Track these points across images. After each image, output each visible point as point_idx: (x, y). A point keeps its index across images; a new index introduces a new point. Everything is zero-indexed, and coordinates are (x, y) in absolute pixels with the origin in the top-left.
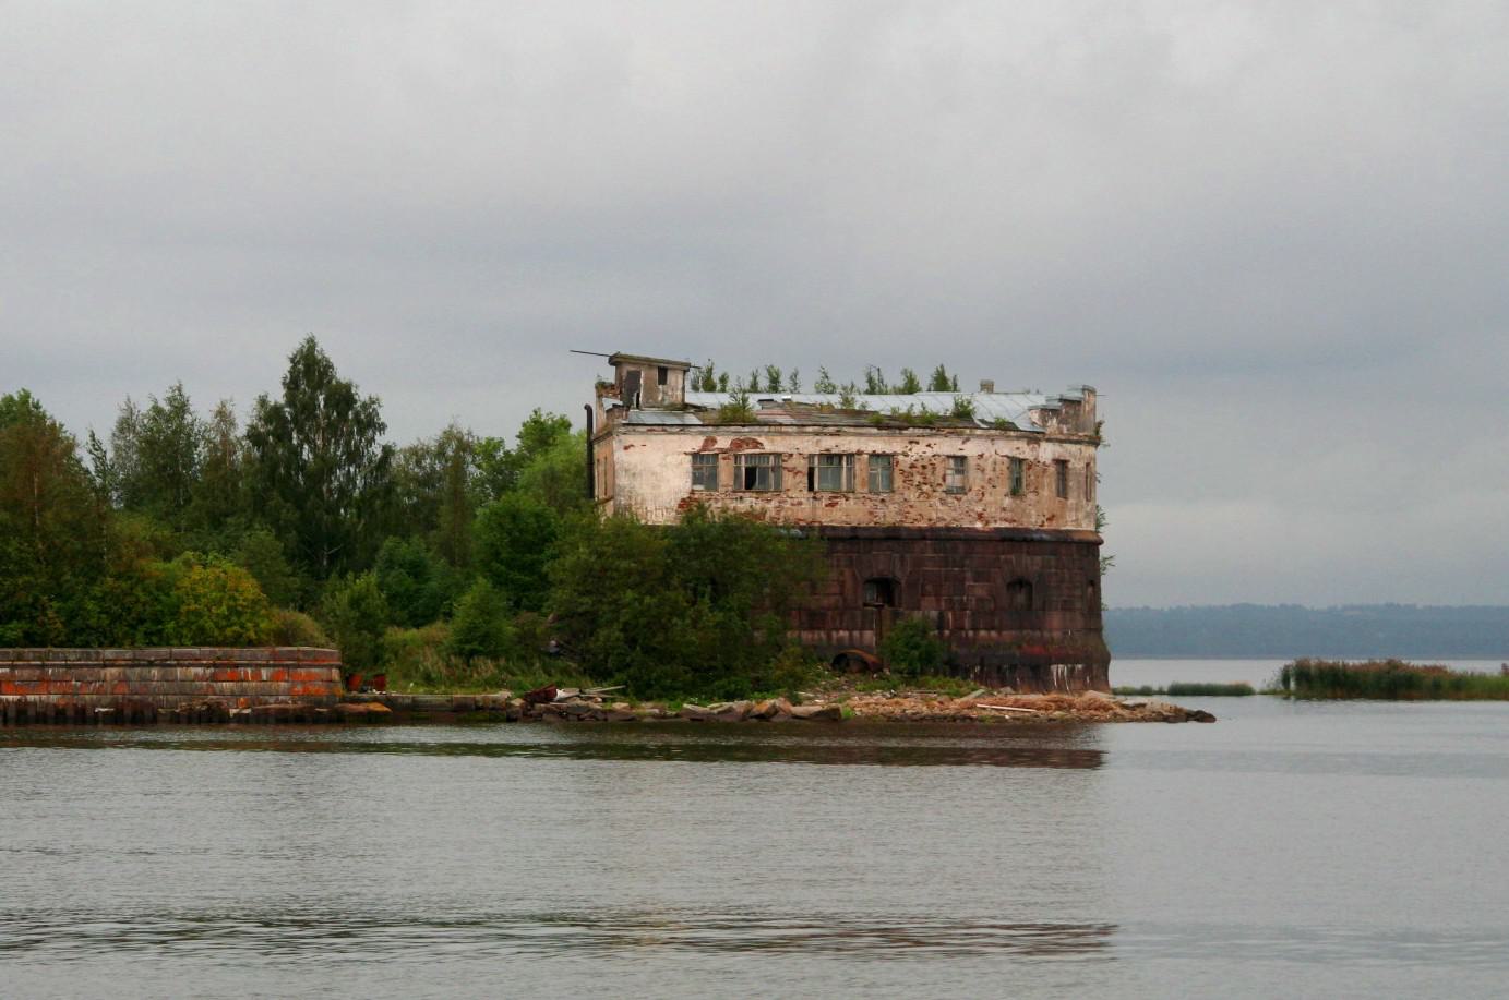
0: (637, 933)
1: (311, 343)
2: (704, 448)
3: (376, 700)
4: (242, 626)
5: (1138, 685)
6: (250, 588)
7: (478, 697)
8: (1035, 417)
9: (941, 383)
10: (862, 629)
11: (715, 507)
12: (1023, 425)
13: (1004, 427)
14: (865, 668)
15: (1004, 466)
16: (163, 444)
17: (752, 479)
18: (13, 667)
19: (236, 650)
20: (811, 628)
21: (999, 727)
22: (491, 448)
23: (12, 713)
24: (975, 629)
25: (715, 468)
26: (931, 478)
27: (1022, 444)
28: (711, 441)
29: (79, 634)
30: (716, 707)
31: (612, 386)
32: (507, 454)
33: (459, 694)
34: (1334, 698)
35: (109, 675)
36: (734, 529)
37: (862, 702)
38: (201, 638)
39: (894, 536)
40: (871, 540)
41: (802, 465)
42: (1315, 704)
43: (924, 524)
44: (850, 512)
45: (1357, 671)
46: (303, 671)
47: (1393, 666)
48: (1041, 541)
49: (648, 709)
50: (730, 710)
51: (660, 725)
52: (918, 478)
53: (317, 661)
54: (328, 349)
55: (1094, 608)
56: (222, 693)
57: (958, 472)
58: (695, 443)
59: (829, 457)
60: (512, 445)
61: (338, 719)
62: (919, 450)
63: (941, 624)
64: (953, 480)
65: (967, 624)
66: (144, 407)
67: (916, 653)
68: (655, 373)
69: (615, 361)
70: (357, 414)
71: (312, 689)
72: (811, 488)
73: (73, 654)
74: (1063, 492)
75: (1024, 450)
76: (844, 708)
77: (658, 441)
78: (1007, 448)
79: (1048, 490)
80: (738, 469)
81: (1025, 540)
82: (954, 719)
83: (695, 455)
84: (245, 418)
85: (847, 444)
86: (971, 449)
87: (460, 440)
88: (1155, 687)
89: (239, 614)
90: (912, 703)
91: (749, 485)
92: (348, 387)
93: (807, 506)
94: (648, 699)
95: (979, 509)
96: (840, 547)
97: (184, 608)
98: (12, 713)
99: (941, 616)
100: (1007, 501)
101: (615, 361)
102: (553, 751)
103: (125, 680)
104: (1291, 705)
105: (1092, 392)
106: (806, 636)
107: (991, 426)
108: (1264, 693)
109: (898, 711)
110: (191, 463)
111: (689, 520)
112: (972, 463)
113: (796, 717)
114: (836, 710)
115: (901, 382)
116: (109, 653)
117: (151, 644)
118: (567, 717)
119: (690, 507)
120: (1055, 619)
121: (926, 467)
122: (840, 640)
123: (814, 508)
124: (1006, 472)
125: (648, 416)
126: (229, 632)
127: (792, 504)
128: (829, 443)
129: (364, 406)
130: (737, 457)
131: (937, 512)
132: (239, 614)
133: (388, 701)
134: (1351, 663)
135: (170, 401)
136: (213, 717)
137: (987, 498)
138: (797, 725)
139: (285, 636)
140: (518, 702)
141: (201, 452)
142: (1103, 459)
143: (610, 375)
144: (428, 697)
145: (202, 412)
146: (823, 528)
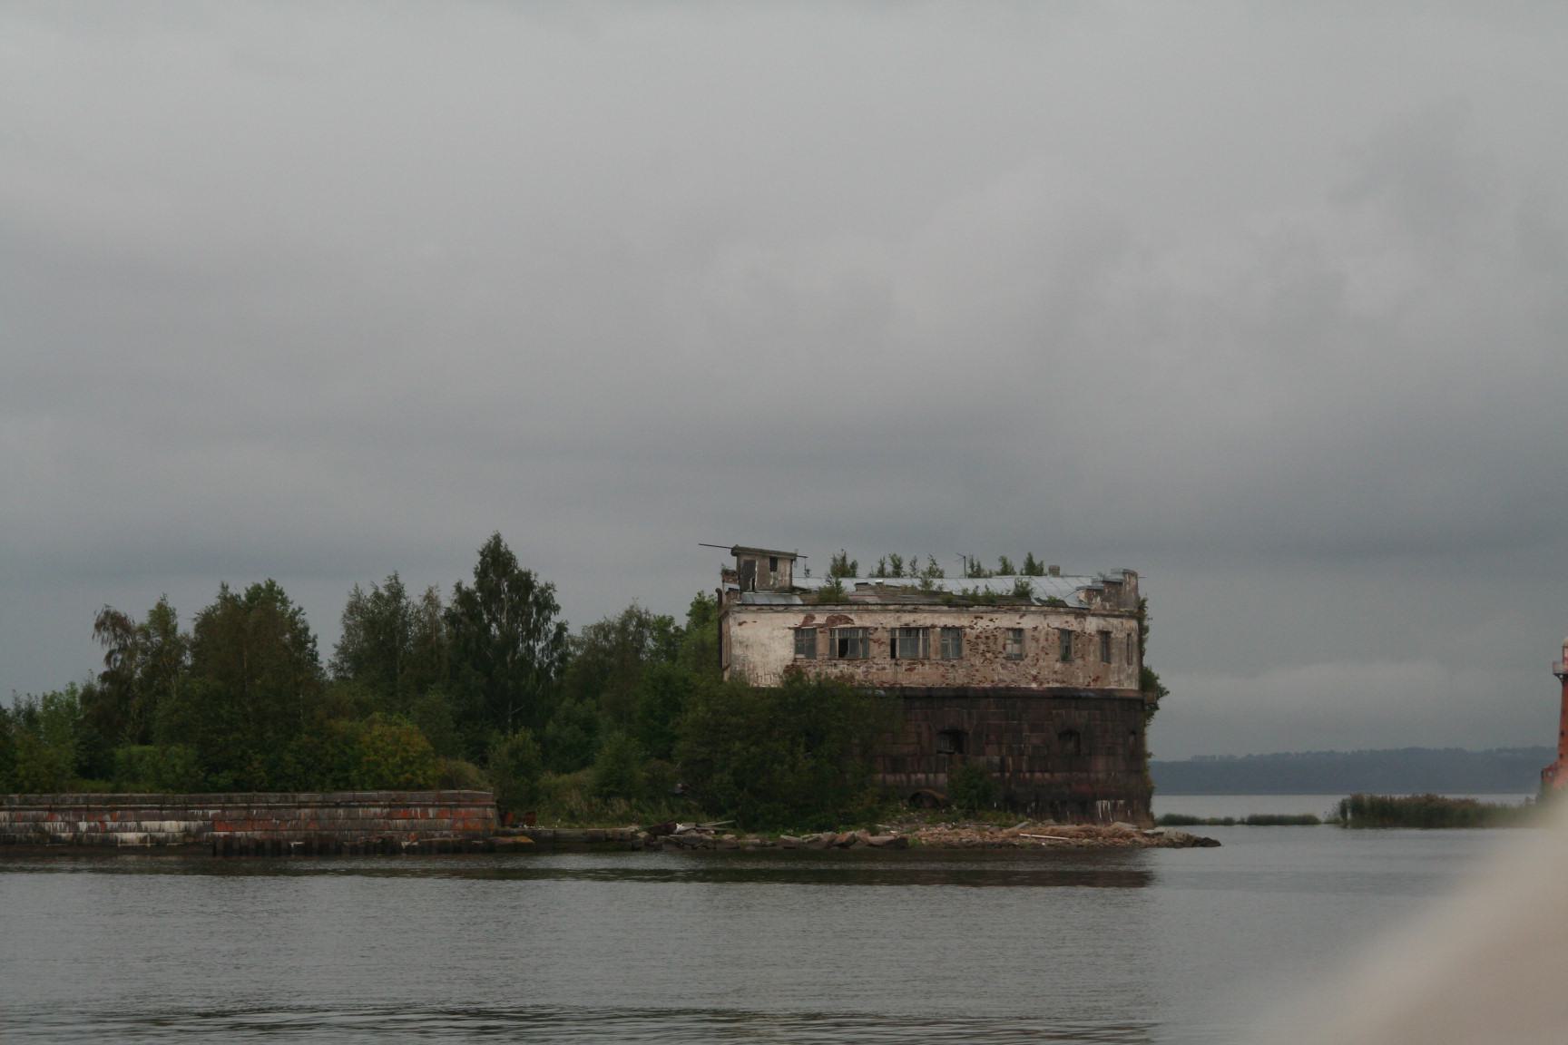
0: (791, 1021)
1: (497, 539)
2: (805, 623)
3: (523, 834)
4: (413, 773)
5: (1222, 816)
6: (420, 743)
7: (609, 830)
8: (1082, 596)
9: (1006, 571)
10: (936, 772)
11: (812, 672)
12: (1072, 603)
13: (1055, 605)
14: (935, 804)
15: (1055, 638)
16: (380, 623)
18: (223, 809)
19: (408, 793)
20: (894, 771)
21: (1037, 852)
22: (663, 624)
23: (220, 847)
24: (1032, 771)
25: (814, 640)
26: (993, 647)
27: (1071, 619)
28: (810, 618)
29: (280, 781)
30: (806, 837)
31: (733, 573)
32: (677, 629)
33: (595, 828)
34: (1384, 826)
35: (303, 814)
36: (826, 691)
37: (930, 833)
38: (380, 784)
39: (962, 695)
40: (944, 698)
41: (886, 637)
42: (1368, 832)
43: (987, 685)
44: (925, 675)
45: (1403, 804)
46: (463, 810)
47: (1430, 799)
48: (1087, 698)
49: (752, 839)
50: (818, 840)
51: (762, 852)
52: (982, 647)
53: (473, 801)
54: (511, 543)
55: (1137, 755)
56: (396, 829)
57: (1016, 642)
58: (797, 619)
59: (908, 630)
60: (682, 621)
61: (490, 849)
62: (983, 624)
63: (1002, 767)
64: (1012, 648)
65: (1024, 767)
66: (369, 593)
67: (974, 792)
68: (767, 561)
69: (736, 552)
70: (536, 598)
71: (471, 825)
72: (893, 656)
73: (273, 797)
74: (1106, 657)
75: (1073, 624)
76: (911, 838)
77: (766, 618)
78: (1056, 622)
79: (1093, 657)
80: (833, 640)
81: (1073, 698)
82: (1000, 846)
83: (797, 630)
84: (447, 599)
85: (924, 619)
86: (1027, 623)
87: (640, 619)
88: (1237, 818)
89: (411, 763)
90: (968, 833)
92: (528, 575)
93: (890, 671)
94: (754, 831)
95: (1034, 672)
96: (917, 704)
97: (365, 759)
98: (220, 847)
99: (1002, 761)
100: (1058, 666)
101: (736, 552)
102: (690, 877)
103: (315, 819)
104: (1350, 833)
105: (1134, 574)
106: (890, 778)
107: (1044, 603)
108: (1242, 822)
109: (956, 840)
110: (405, 639)
111: (788, 684)
112: (1028, 634)
113: (871, 845)
114: (904, 840)
115: (998, 567)
116: (303, 796)
117: (338, 789)
118: (682, 846)
119: (793, 673)
120: (1100, 764)
121: (989, 637)
122: (918, 781)
123: (896, 673)
124: (1057, 643)
125: (761, 599)
126: (402, 778)
127: (879, 670)
128: (908, 619)
129: (543, 591)
130: (832, 631)
131: (1000, 675)
132: (411, 763)
133: (534, 835)
134: (1397, 797)
135: (388, 587)
136: (388, 848)
137: (1041, 663)
138: (874, 851)
139: (450, 781)
140: (643, 835)
141: (414, 630)
143: (732, 563)
144: (568, 831)
145: (414, 596)
146: (903, 689)
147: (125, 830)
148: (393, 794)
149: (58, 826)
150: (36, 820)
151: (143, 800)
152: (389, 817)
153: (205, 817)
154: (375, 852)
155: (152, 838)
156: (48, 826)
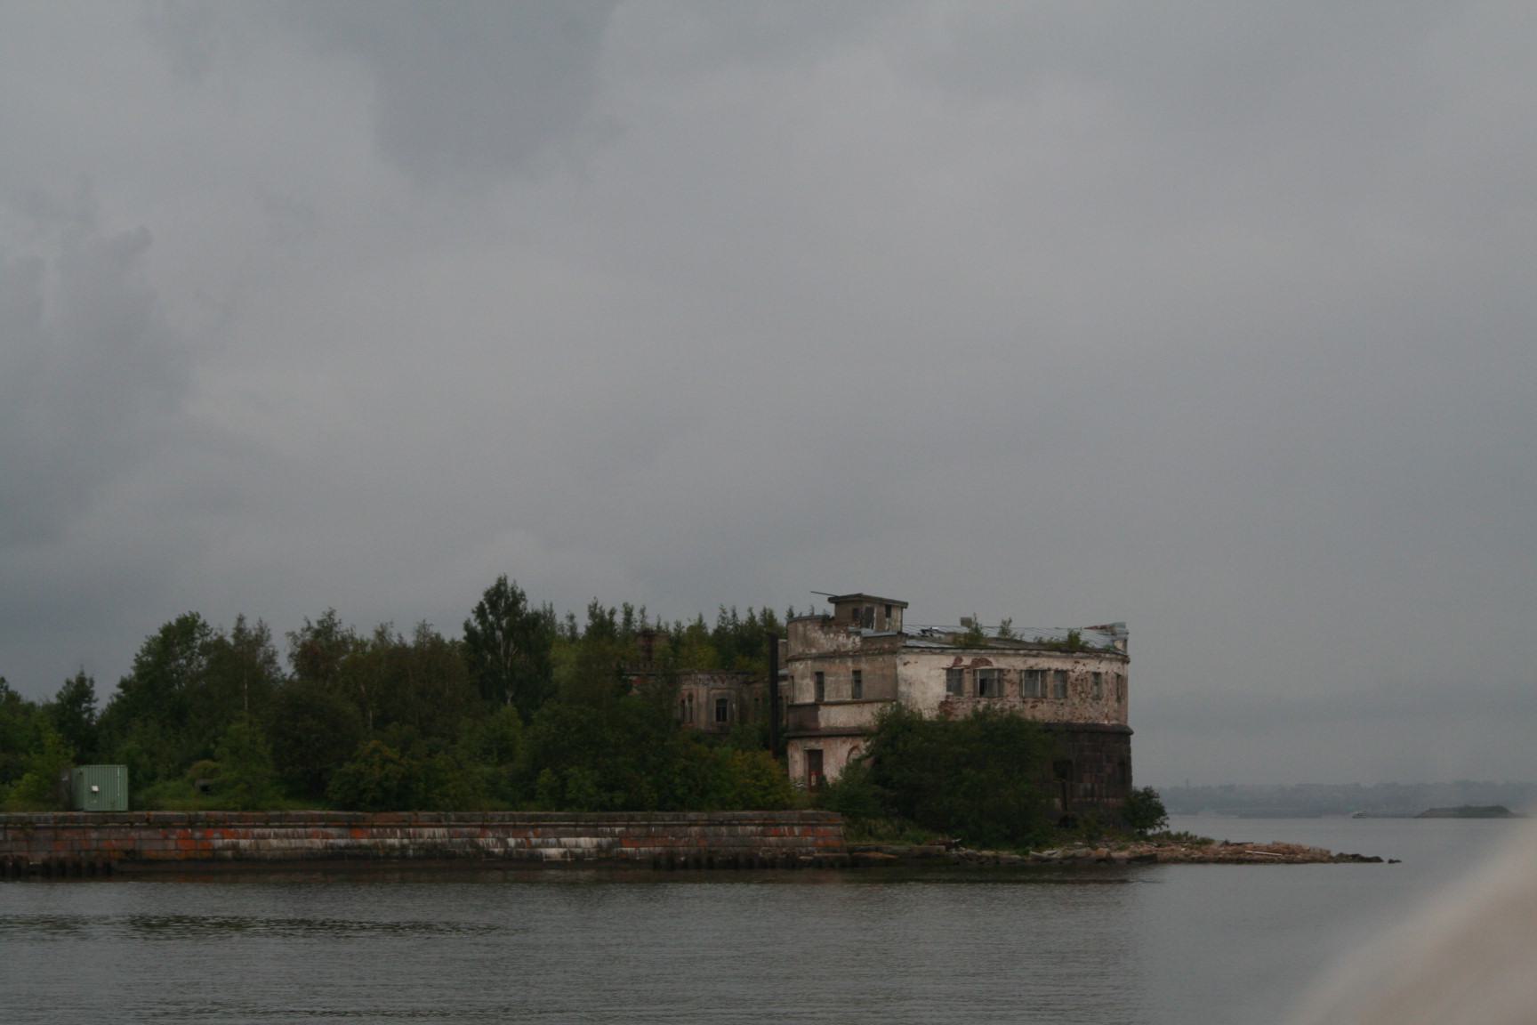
17: (983, 688)
18: (628, 826)
28: (959, 660)
29: (670, 801)
35: (693, 832)
44: (1045, 712)
46: (821, 829)
54: (520, 580)
58: (948, 661)
59: (1031, 673)
77: (926, 659)
83: (949, 671)
85: (1043, 663)
91: (982, 693)
103: (704, 836)
116: (692, 815)
121: (1082, 680)
128: (1032, 662)
142: (1130, 671)
147: (548, 846)
148: (765, 814)
149: (489, 841)
150: (471, 836)
151: (560, 819)
152: (764, 834)
153: (612, 834)
154: (34, 873)
155: (572, 855)
156: (481, 841)
